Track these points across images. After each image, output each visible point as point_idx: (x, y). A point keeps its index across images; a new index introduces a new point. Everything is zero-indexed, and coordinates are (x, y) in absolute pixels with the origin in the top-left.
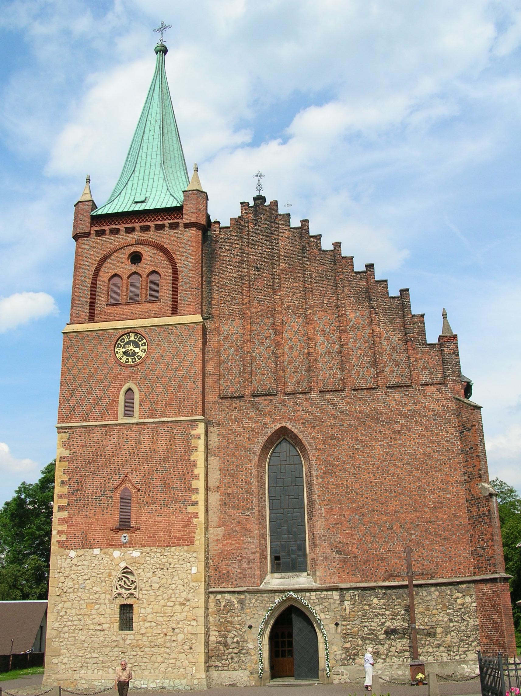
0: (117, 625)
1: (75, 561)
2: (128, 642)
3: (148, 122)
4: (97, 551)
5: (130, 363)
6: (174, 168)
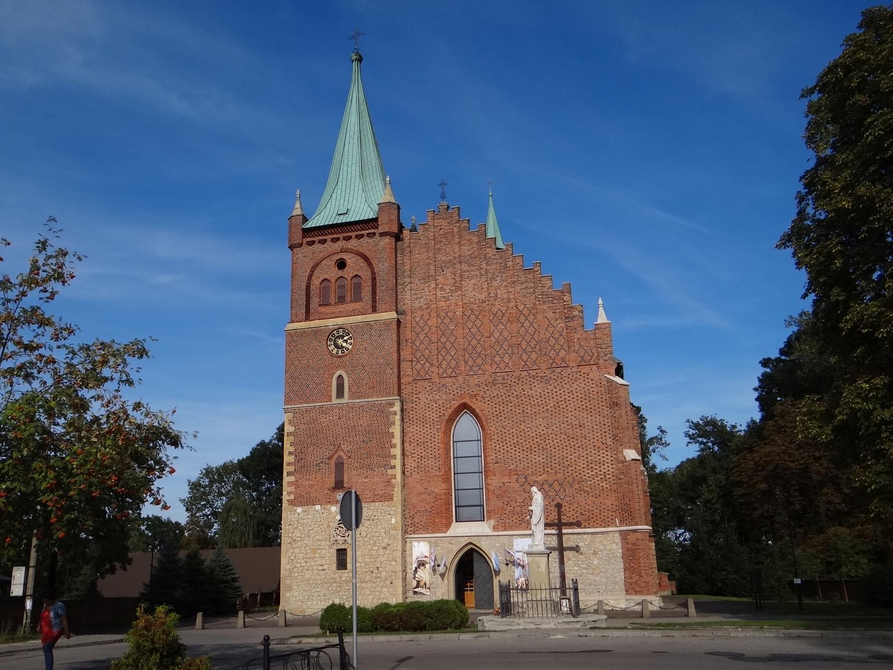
0: (335, 566)
1: (301, 516)
2: (343, 578)
3: (348, 134)
4: (318, 507)
5: (340, 354)
6: (371, 177)
